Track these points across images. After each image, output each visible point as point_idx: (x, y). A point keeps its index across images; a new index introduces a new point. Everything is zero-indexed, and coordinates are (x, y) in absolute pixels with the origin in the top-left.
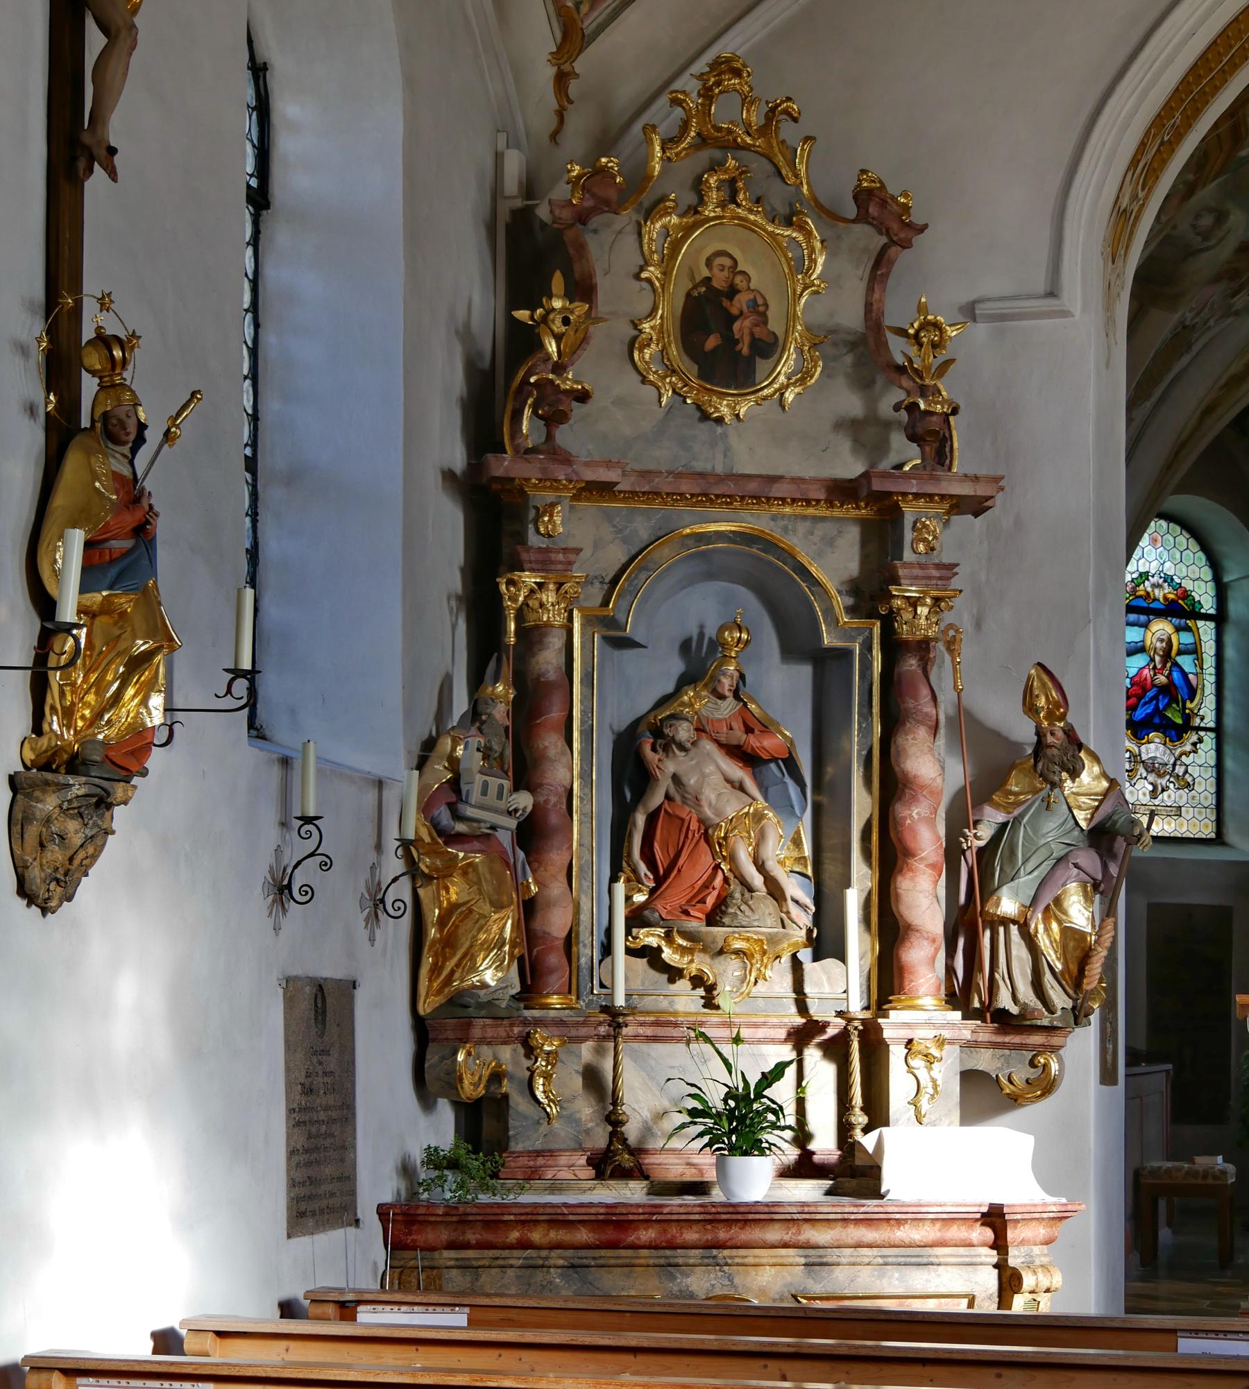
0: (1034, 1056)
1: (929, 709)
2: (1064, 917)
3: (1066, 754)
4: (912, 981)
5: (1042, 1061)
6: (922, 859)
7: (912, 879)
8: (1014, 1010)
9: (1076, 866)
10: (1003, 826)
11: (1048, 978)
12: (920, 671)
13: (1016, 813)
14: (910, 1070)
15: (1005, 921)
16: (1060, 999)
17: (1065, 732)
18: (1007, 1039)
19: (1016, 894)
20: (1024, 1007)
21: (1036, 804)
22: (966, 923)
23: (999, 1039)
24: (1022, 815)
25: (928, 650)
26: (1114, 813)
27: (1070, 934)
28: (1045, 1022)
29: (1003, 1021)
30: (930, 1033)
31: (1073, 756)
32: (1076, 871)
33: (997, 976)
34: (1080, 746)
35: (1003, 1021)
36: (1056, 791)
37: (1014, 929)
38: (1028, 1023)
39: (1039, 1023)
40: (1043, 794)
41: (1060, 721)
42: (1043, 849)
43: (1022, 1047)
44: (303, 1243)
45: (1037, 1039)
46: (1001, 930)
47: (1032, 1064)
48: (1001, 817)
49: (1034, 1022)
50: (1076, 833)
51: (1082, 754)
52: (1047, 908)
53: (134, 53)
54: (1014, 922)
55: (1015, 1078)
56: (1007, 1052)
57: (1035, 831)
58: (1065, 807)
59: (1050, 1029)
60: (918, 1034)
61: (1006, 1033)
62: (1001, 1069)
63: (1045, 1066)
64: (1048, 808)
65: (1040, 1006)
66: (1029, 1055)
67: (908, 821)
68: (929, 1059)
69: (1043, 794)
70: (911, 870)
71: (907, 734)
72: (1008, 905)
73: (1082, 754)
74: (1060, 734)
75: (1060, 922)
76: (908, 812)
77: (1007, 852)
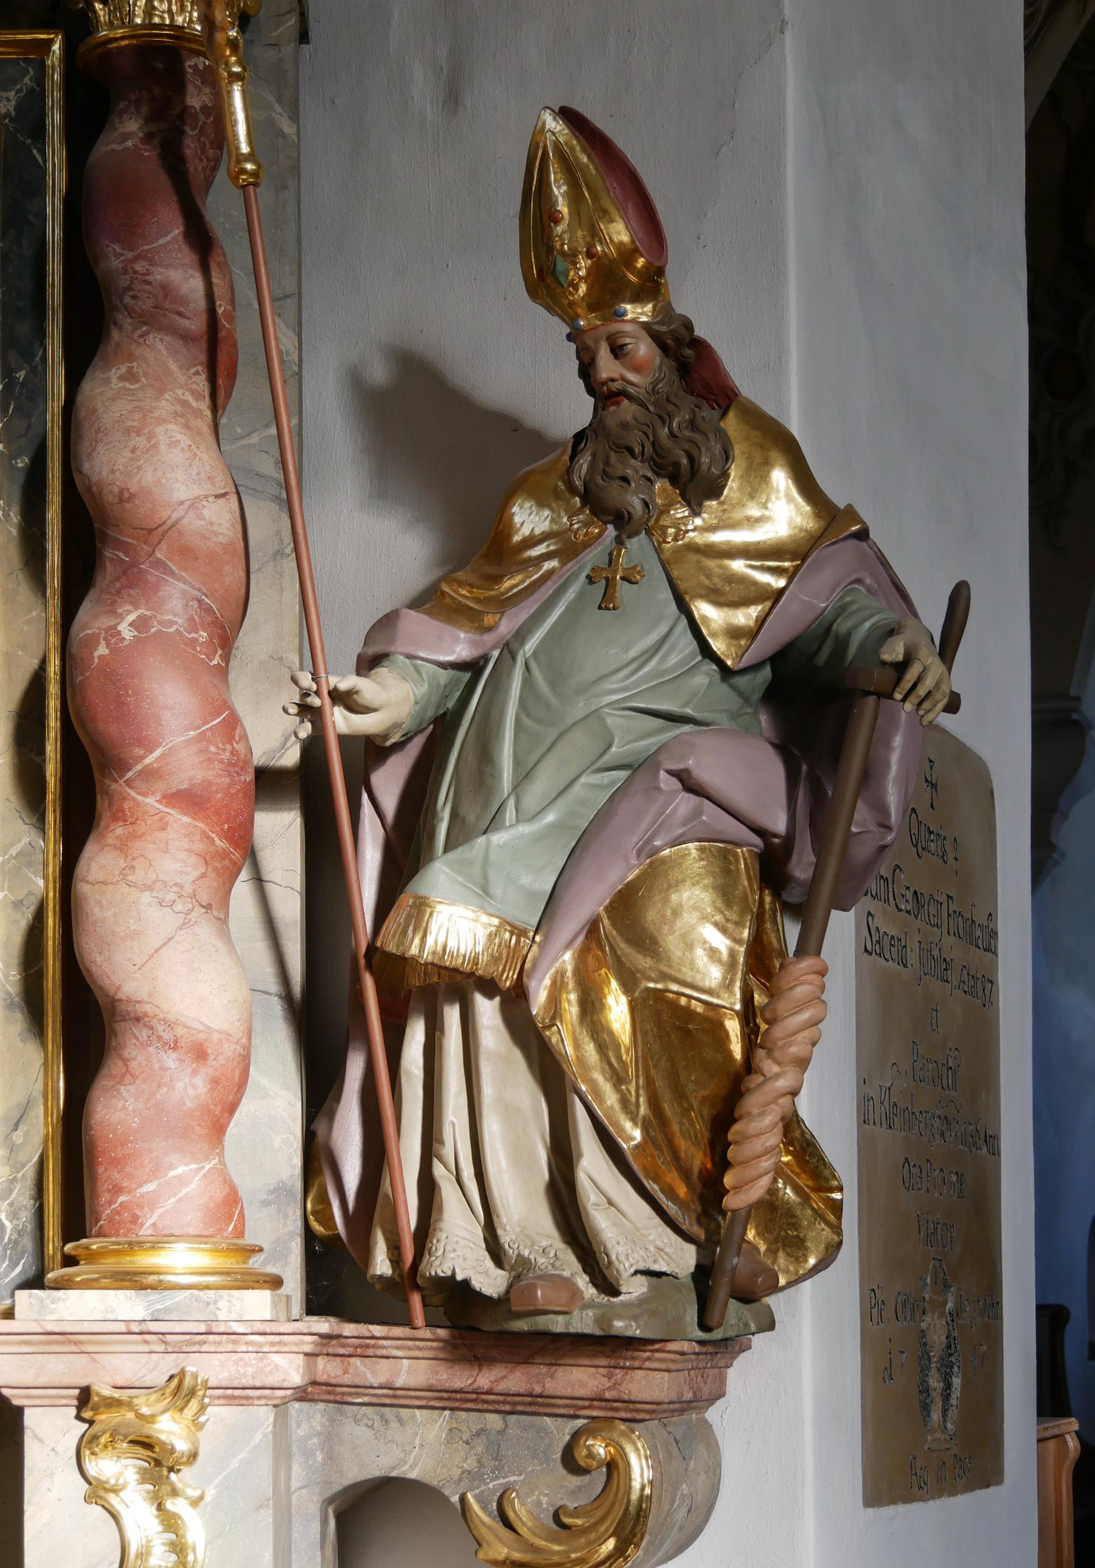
0: (576, 1436)
1: (189, 283)
2: (643, 962)
3: (664, 418)
4: (117, 1190)
5: (601, 1450)
6: (149, 774)
7: (123, 847)
8: (490, 1281)
9: (689, 784)
10: (473, 667)
11: (593, 1166)
12: (149, 153)
13: (507, 626)
14: (97, 1492)
15: (457, 984)
16: (638, 1237)
17: (657, 338)
18: (485, 1379)
19: (482, 892)
20: (520, 1270)
21: (570, 595)
22: (348, 1002)
23: (460, 1378)
24: (522, 635)
25: (176, 81)
26: (841, 610)
27: (673, 1025)
28: (583, 1322)
29: (470, 1323)
30: (156, 1369)
31: (693, 425)
32: (685, 803)
33: (438, 1170)
34: (721, 395)
35: (470, 1323)
36: (637, 544)
37: (487, 1009)
38: (522, 1325)
39: (558, 1324)
40: (594, 556)
41: (638, 298)
42: (577, 737)
43: (535, 1404)
44: (870, 1511)
45: (580, 1378)
46: (452, 1015)
47: (570, 1462)
48: (461, 646)
49: (542, 1322)
50: (705, 676)
51: (731, 424)
52: (593, 929)
53: (576, 364)
54: (489, 987)
55: (520, 1510)
56: (494, 1421)
57: (557, 681)
58: (667, 594)
59: (607, 1345)
60: (109, 1373)
61: (479, 1361)
62: (474, 1477)
63: (611, 1466)
64: (608, 602)
65: (570, 1265)
66: (562, 1431)
67: (102, 650)
68: (159, 1463)
69: (594, 556)
70: (119, 816)
71: (108, 367)
72: (455, 925)
73: (731, 424)
74: (643, 349)
75: (628, 983)
76: (107, 622)
77: (471, 758)
